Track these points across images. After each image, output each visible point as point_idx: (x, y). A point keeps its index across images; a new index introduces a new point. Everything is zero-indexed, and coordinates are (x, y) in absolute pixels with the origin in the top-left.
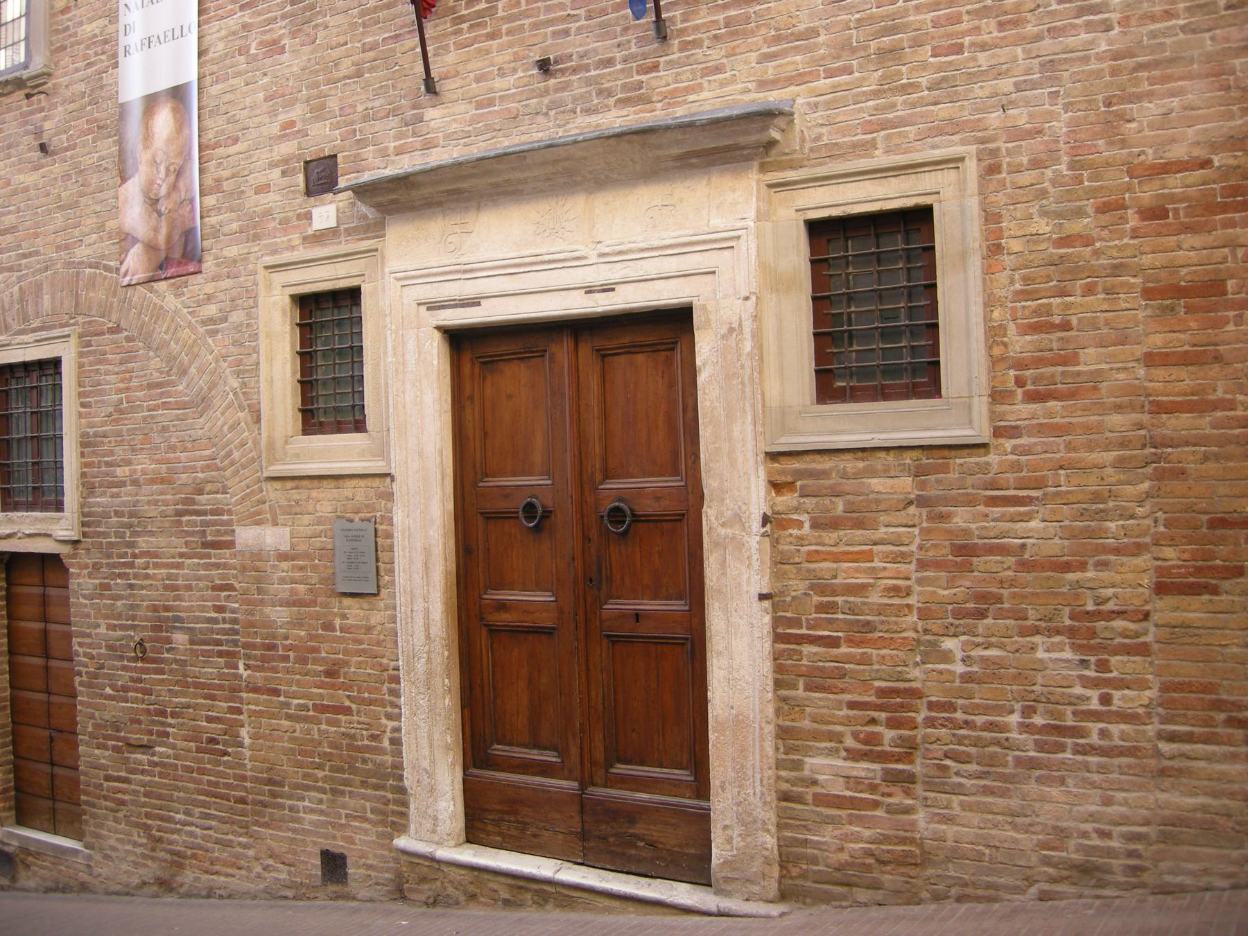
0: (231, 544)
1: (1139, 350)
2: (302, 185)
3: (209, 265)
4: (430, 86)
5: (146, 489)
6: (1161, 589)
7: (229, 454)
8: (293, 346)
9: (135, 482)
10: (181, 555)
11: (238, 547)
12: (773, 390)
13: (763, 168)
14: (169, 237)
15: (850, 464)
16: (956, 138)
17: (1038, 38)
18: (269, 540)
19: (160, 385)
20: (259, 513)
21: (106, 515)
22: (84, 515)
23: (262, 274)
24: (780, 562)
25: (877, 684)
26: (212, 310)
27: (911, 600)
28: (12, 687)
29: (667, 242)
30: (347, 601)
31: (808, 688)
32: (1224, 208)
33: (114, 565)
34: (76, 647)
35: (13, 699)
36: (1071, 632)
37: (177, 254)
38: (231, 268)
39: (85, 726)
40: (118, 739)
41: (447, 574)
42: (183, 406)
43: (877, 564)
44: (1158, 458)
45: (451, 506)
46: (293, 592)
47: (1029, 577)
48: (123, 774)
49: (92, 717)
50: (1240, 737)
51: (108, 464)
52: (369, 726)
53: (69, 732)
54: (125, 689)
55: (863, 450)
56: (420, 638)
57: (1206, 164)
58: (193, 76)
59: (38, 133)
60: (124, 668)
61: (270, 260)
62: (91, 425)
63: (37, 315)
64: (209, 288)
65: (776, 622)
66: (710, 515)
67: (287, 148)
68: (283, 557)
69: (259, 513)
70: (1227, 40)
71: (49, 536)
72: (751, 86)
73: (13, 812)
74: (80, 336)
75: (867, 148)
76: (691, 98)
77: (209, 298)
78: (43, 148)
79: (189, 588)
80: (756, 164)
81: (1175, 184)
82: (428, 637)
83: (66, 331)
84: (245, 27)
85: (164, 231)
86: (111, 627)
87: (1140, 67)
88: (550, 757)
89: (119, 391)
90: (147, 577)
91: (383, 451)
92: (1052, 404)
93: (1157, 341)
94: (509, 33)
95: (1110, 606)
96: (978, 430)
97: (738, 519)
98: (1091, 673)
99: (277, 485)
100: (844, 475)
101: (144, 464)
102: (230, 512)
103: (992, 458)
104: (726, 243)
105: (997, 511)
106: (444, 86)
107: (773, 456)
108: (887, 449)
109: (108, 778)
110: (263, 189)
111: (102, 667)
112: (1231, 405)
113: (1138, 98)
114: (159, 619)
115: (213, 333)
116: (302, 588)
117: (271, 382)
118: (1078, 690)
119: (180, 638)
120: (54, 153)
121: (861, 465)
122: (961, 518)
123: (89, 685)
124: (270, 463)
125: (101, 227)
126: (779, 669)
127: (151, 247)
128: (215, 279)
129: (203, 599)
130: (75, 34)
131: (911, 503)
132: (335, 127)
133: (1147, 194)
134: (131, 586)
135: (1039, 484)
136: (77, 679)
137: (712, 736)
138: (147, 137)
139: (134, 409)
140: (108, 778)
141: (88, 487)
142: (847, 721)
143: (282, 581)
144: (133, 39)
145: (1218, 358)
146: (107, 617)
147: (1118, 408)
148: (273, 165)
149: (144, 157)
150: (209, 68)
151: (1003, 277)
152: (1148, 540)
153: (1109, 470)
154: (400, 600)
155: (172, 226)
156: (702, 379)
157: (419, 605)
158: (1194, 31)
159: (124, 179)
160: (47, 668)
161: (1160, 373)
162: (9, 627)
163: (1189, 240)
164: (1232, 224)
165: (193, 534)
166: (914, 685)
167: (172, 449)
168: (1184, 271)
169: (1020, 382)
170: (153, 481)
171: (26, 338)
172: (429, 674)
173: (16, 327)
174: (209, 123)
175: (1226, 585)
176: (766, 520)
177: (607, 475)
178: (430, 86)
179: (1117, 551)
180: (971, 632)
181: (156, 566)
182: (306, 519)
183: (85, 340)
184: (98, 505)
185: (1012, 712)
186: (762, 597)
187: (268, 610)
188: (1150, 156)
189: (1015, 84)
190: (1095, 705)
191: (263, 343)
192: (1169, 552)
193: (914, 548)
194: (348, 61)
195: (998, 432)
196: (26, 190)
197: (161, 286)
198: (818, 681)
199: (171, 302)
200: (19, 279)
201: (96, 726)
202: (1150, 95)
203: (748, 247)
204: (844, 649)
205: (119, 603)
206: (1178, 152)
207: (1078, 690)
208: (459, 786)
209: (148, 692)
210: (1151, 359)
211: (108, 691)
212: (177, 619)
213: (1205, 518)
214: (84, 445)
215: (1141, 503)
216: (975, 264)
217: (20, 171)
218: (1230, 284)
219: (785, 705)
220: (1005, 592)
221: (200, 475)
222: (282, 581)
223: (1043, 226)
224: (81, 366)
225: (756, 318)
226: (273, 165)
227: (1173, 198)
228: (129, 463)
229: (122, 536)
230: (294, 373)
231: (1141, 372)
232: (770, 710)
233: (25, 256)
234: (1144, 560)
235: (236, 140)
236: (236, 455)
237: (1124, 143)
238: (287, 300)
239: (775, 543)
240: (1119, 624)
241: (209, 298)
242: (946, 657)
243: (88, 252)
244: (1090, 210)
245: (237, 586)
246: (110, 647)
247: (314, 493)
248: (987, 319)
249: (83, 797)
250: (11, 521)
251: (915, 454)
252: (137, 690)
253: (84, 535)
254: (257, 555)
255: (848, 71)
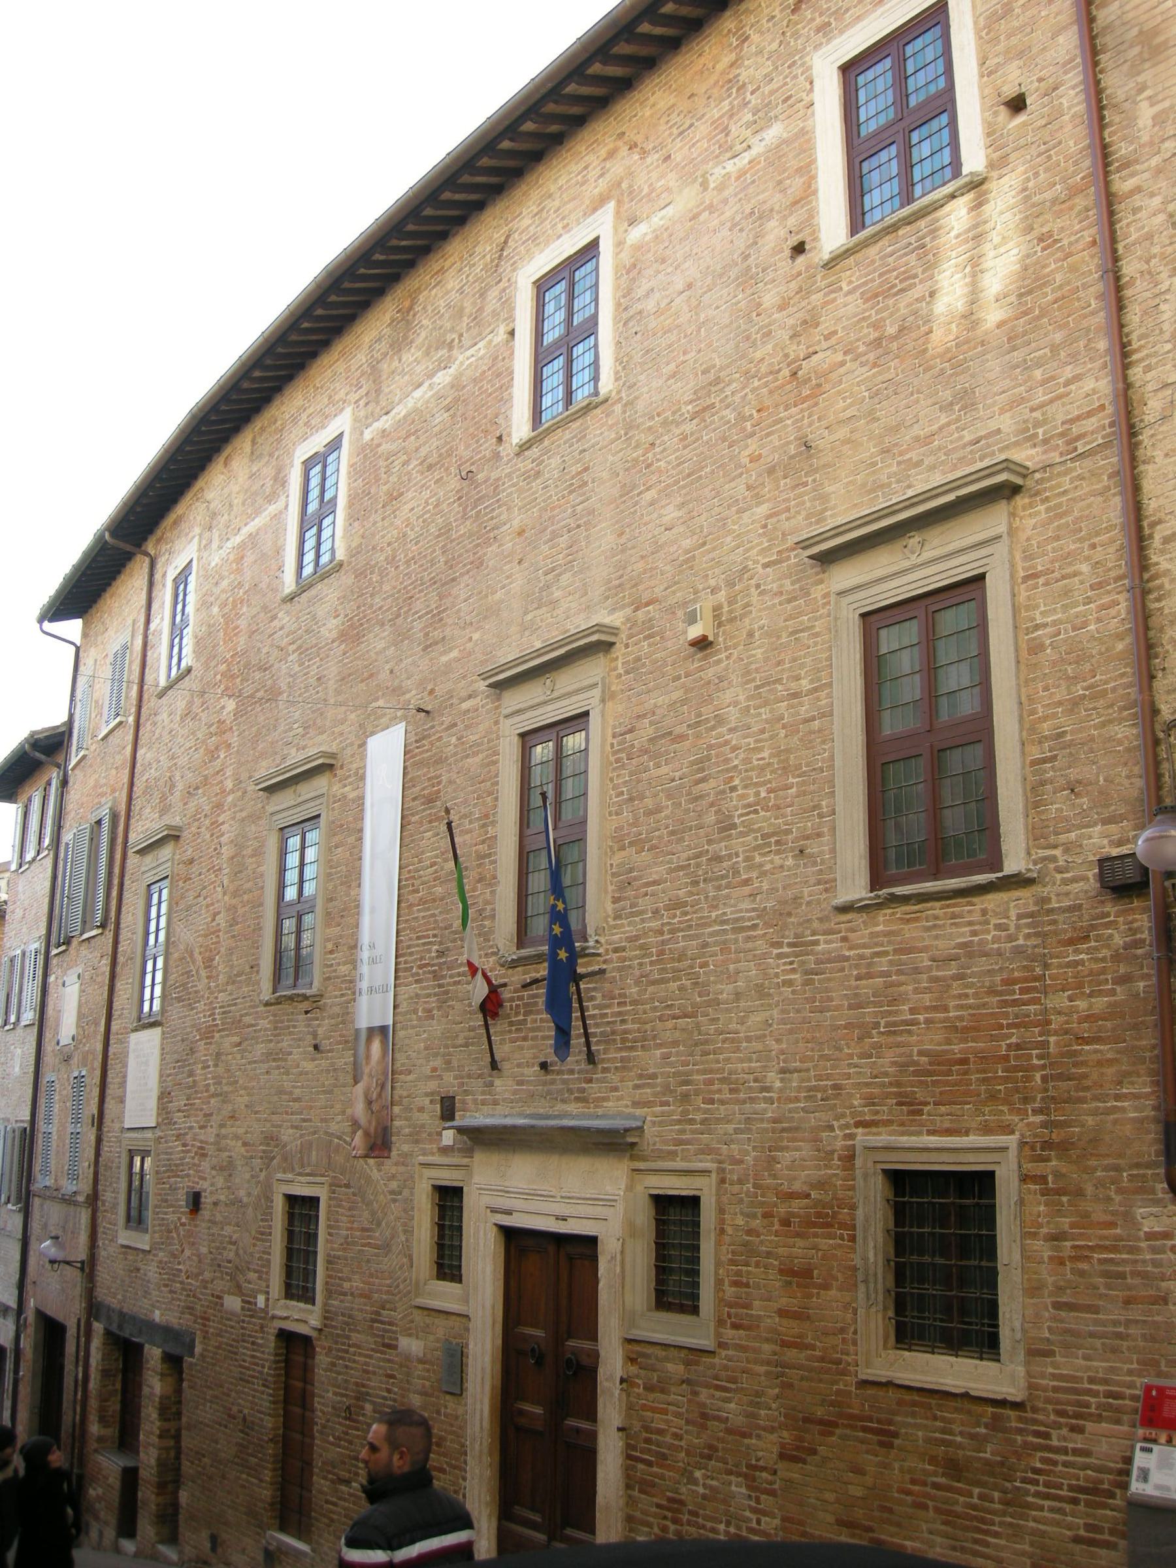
0: (395, 1347)
1: (776, 1306)
2: (439, 1113)
3: (394, 1153)
4: (494, 1065)
5: (357, 1300)
6: (782, 1456)
7: (398, 1286)
8: (432, 1219)
9: (352, 1294)
10: (373, 1350)
11: (399, 1350)
12: (628, 1298)
13: (633, 1158)
14: (376, 1129)
15: (660, 1353)
16: (709, 1157)
17: (744, 1102)
18: (414, 1348)
19: (367, 1230)
20: (410, 1329)
21: (336, 1314)
22: (327, 1311)
23: (417, 1167)
24: (630, 1407)
25: (668, 1494)
26: (394, 1185)
27: (682, 1443)
28: (285, 1427)
29: (588, 1196)
30: (448, 1397)
31: (641, 1491)
32: (815, 1225)
33: (339, 1350)
34: (316, 1405)
35: (284, 1436)
36: (746, 1476)
37: (379, 1142)
38: (405, 1157)
39: (318, 1463)
40: (334, 1474)
41: (493, 1388)
42: (377, 1247)
43: (670, 1417)
44: (783, 1375)
45: (499, 1342)
46: (424, 1386)
47: (730, 1438)
48: (334, 1500)
49: (321, 1456)
50: (270, 1425)
51: (340, 1278)
52: (454, 1484)
53: (308, 1464)
54: (339, 1439)
55: (665, 1345)
56: (477, 1429)
57: (808, 1196)
58: (391, 1023)
59: (315, 1035)
60: (340, 1424)
61: (421, 1159)
62: (332, 1249)
63: (309, 1165)
64: (393, 1170)
65: (629, 1446)
66: (601, 1371)
67: (432, 1085)
68: (421, 1361)
69: (410, 1329)
70: (820, 1120)
71: (306, 1322)
72: (629, 1103)
73: (278, 1521)
74: (331, 1185)
75: (672, 1155)
76: (605, 1104)
77: (393, 1177)
78: (316, 1047)
79: (374, 1373)
80: (628, 1155)
81: (796, 1206)
82: (481, 1428)
83: (323, 1179)
84: (417, 996)
85: (374, 1124)
86: (335, 1394)
87: (783, 1130)
88: (537, 1518)
89: (348, 1229)
90: (354, 1361)
91: (466, 1300)
92: (741, 1332)
93: (784, 1302)
94: (532, 1039)
95: (761, 1463)
96: (707, 1343)
97: (610, 1378)
98: (753, 1504)
99: (420, 1312)
100: (657, 1358)
101: (357, 1283)
102: (397, 1325)
103: (717, 1360)
104: (610, 1203)
105: (718, 1394)
106: (505, 1066)
107: (630, 1341)
108: (675, 1346)
109: (327, 1502)
110: (421, 1109)
111: (328, 1421)
112: (813, 1348)
113: (781, 1149)
114: (359, 1392)
115: (395, 1201)
116: (427, 1383)
117: (419, 1241)
118: (748, 1514)
119: (368, 1407)
120: (322, 1052)
121: (664, 1353)
122: (704, 1395)
123: (321, 1433)
124: (416, 1296)
125: (343, 1113)
126: (628, 1477)
127: (367, 1134)
128: (396, 1164)
129: (381, 1382)
130: (335, 971)
131: (683, 1382)
132: (456, 1078)
133: (782, 1210)
134: (347, 1367)
135: (733, 1380)
136: (316, 1428)
137: (598, 1515)
138: (368, 1057)
139: (354, 1243)
140: (327, 1502)
141: (329, 1293)
142: (655, 1515)
143: (419, 1377)
144: (364, 985)
145: (808, 1318)
146: (334, 1386)
147: (767, 1340)
148: (427, 1095)
149: (367, 1070)
150: (399, 1018)
151: (724, 1248)
152: (776, 1424)
153: (763, 1378)
154: (469, 1401)
155: (378, 1123)
156: (601, 1285)
157: (478, 1406)
158: (807, 1112)
159: (356, 1082)
160: (303, 1416)
161: (785, 1322)
162: (285, 1382)
163: (800, 1242)
164: (816, 1235)
165: (378, 1336)
166: (683, 1497)
167: (371, 1275)
168: (796, 1261)
169: (729, 1316)
170: (361, 1295)
171: (302, 1179)
172: (481, 1451)
173: (298, 1170)
174: (397, 1055)
175: (809, 1459)
176: (622, 1381)
177: (570, 1336)
178: (494, 1065)
179: (764, 1429)
180: (706, 1468)
181: (360, 1355)
182: (431, 1338)
183: (334, 1185)
184: (333, 1306)
185: (721, 1522)
186: (619, 1429)
187: (411, 1395)
188: (785, 1188)
189: (735, 1129)
190: (754, 1525)
191: (416, 1213)
192: (785, 1434)
193: (684, 1410)
194: (462, 1035)
195: (721, 1345)
196: (307, 1073)
197: (371, 1161)
198: (646, 1486)
199: (375, 1175)
200: (302, 1136)
201: (323, 1463)
202: (787, 1148)
203: (620, 1207)
204: (655, 1469)
205: (340, 1377)
206: (797, 1186)
207: (748, 1514)
208: (494, 1531)
209: (351, 1443)
210: (782, 1313)
211: (331, 1439)
212: (368, 1394)
213: (801, 1415)
214: (329, 1262)
215: (774, 1401)
216: (713, 1235)
217: (305, 1059)
218: (816, 1272)
219: (631, 1502)
220: (720, 1446)
221: (384, 1297)
222: (419, 1377)
223: (740, 1221)
224: (330, 1206)
225: (622, 1252)
226: (427, 1095)
227: (793, 1215)
228: (350, 1280)
229: (344, 1330)
230: (432, 1237)
231: (777, 1319)
232: (622, 1502)
233: (304, 1120)
234: (773, 1437)
235: (410, 1072)
236: (401, 1287)
237: (775, 1177)
238: (430, 1188)
239: (628, 1395)
240: (764, 1475)
241: (393, 1177)
242: (695, 1482)
243: (336, 1127)
244: (759, 1215)
245: (398, 1376)
246: (334, 1408)
247: (436, 1321)
248: (716, 1273)
249: (313, 1514)
250: (287, 1307)
251: (686, 1352)
252: (346, 1441)
253: (325, 1326)
254: (408, 1357)
255: (667, 1104)
